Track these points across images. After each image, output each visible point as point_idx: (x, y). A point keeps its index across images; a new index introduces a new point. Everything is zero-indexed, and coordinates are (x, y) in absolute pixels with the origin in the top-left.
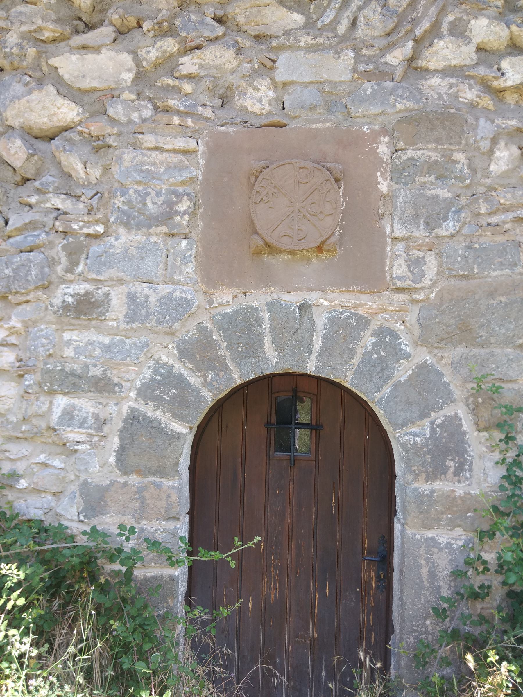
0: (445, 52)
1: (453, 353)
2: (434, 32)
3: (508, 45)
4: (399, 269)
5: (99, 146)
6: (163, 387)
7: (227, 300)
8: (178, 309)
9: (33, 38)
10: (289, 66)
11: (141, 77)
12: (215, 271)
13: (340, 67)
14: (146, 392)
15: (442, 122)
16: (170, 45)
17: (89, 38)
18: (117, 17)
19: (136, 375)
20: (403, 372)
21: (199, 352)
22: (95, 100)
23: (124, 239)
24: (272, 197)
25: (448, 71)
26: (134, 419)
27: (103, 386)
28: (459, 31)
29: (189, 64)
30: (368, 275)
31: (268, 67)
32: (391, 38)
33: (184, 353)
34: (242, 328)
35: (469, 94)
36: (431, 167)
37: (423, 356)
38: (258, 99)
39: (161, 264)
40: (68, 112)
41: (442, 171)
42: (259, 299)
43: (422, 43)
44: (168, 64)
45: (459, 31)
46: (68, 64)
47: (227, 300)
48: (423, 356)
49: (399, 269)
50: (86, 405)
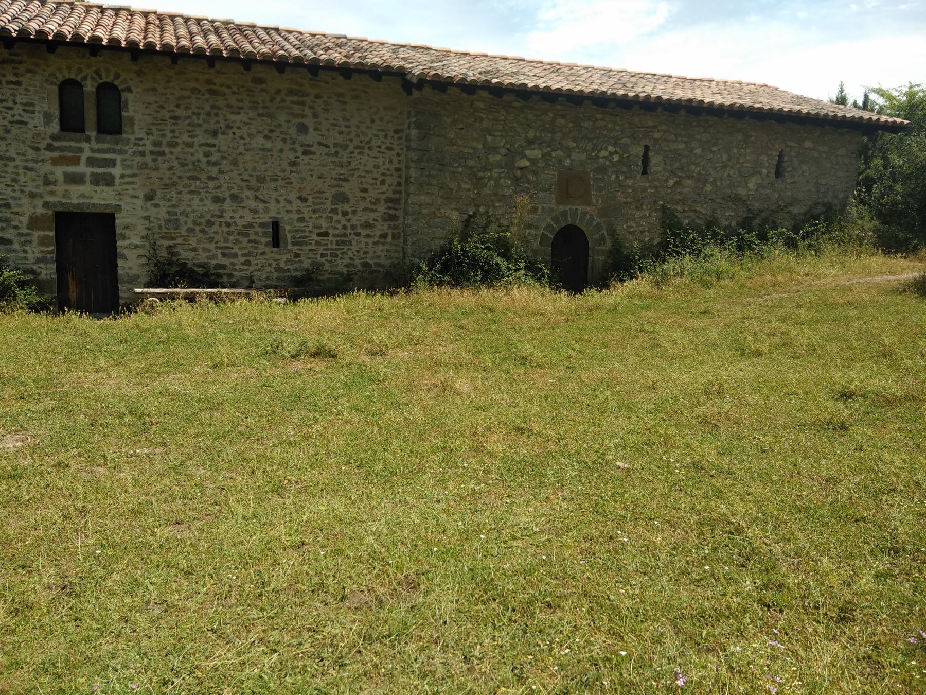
0: (604, 153)
1: (603, 219)
2: (602, 149)
3: (631, 278)
4: (594, 201)
5: (535, 173)
6: (548, 227)
7: (561, 208)
8: (552, 210)
9: (520, 146)
10: (575, 156)
11: (543, 156)
12: (560, 201)
13: (583, 157)
14: (545, 229)
15: (602, 170)
16: (549, 149)
17: (533, 147)
18: (533, 135)
19: (544, 225)
20: (594, 224)
21: (556, 219)
22: (533, 161)
23: (541, 194)
24: (571, 186)
25: (604, 157)
26: (543, 234)
27: (537, 228)
28: (606, 149)
29: (554, 154)
30: (588, 203)
31: (569, 156)
32: (593, 150)
33: (553, 220)
34: (564, 214)
35: (607, 163)
36: (600, 179)
37: (598, 220)
38: (567, 163)
39: (297, 52)
40: (527, 163)
41: (602, 180)
42: (567, 208)
43: (599, 151)
44: (549, 154)
45: (606, 149)
46: (528, 153)
47: (561, 208)
48: (598, 220)
49: (594, 201)
50: (533, 232)
